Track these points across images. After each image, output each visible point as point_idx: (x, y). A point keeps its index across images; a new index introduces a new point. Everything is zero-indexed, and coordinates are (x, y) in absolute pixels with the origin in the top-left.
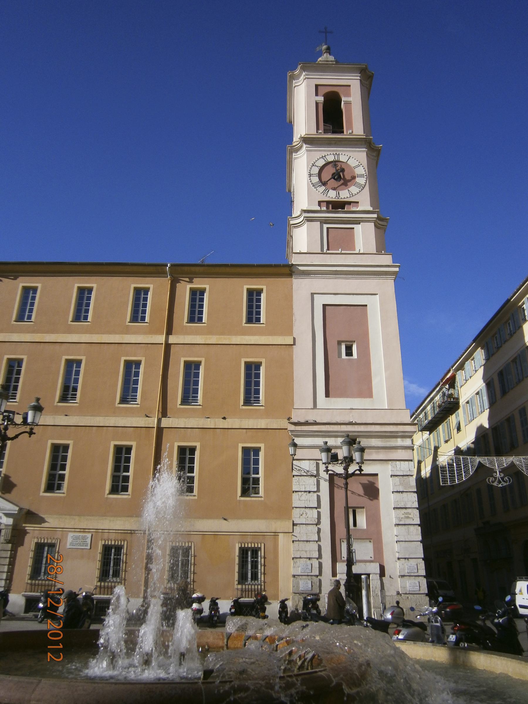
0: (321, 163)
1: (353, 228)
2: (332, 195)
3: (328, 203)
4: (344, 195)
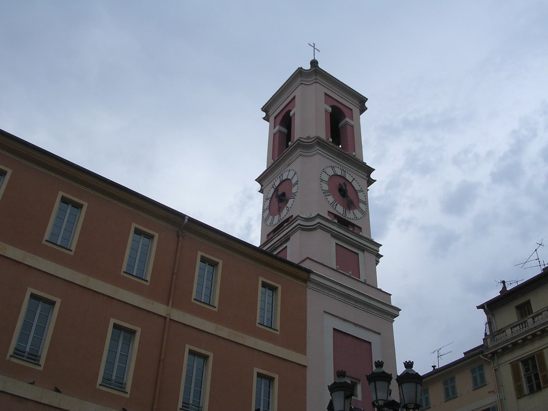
0: (331, 173)
1: (358, 254)
2: (340, 210)
3: (336, 216)
4: (350, 216)
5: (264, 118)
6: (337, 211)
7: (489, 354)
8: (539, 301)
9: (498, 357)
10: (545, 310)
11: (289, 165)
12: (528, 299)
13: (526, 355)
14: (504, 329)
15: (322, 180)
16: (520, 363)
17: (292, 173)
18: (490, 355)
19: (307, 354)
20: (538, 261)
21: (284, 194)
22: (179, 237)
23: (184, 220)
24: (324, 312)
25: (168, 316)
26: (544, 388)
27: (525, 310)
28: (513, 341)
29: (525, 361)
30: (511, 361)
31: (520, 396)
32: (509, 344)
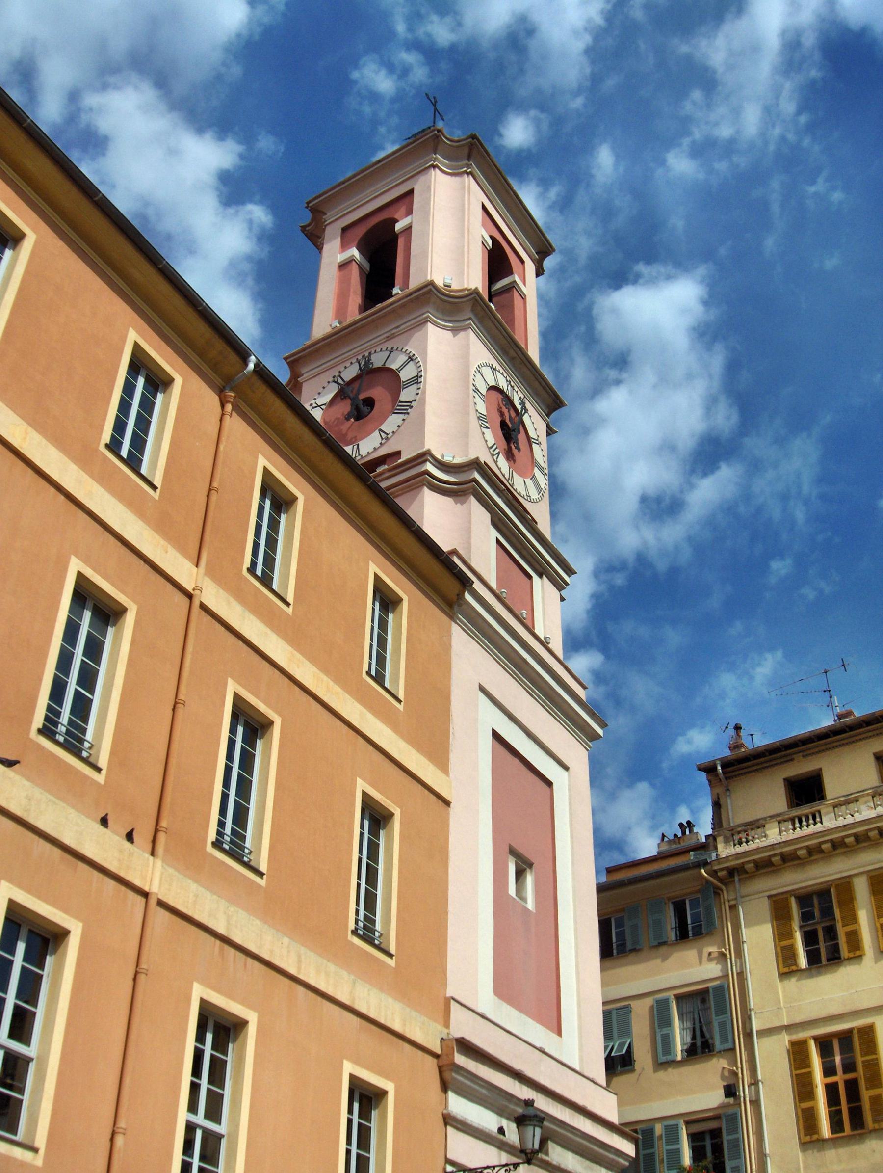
5: (303, 229)
6: (499, 469)
7: (722, 869)
8: (846, 773)
9: (740, 880)
10: (868, 794)
11: (389, 338)
12: (817, 767)
13: (810, 883)
14: (762, 822)
15: (476, 390)
16: (793, 900)
17: (403, 358)
18: (724, 873)
19: (451, 775)
20: (827, 694)
21: (370, 403)
22: (223, 406)
23: (247, 365)
24: (482, 689)
25: (197, 592)
26: (849, 959)
27: (806, 792)
28: (785, 850)
29: (804, 899)
30: (774, 892)
31: (786, 970)
32: (775, 855)
